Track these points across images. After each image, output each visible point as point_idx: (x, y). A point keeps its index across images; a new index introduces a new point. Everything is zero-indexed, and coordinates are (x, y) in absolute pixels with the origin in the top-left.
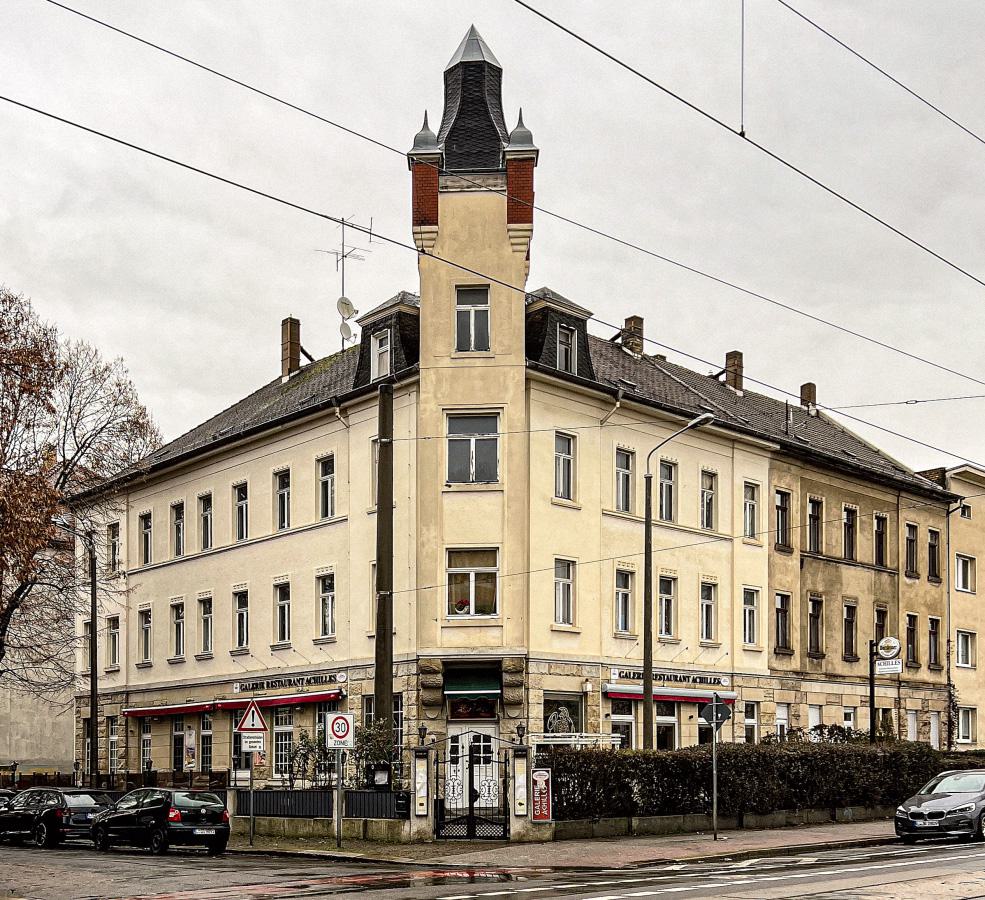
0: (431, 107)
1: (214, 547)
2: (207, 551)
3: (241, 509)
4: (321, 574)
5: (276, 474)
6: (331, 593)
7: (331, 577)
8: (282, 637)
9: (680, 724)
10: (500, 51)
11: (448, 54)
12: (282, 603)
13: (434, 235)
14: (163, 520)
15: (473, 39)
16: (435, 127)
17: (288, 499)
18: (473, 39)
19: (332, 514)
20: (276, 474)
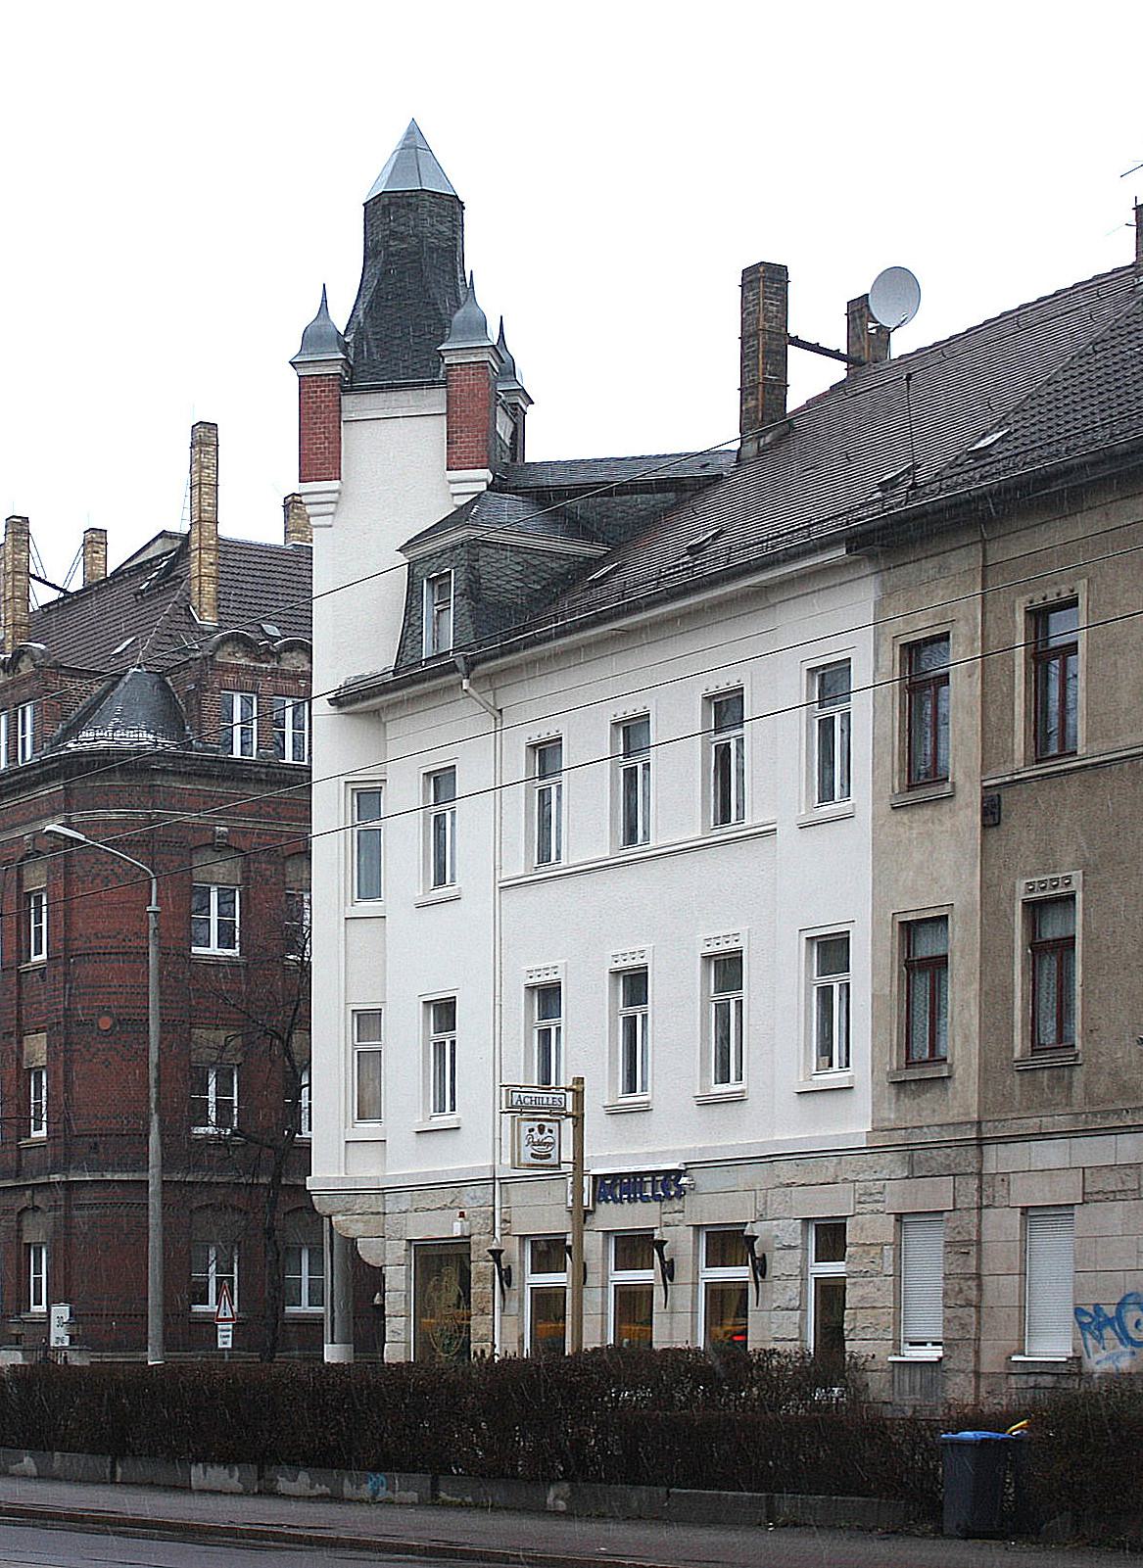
0: (335, 271)
1: (564, 863)
2: (634, 852)
3: (723, 753)
4: (714, 949)
5: (708, 699)
6: (842, 976)
7: (376, 1014)
8: (631, 1088)
9: (696, 1264)
10: (461, 171)
11: (367, 173)
12: (723, 996)
13: (331, 508)
14: (589, 743)
15: (414, 147)
16: (340, 319)
17: (559, 798)
18: (414, 147)
19: (741, 817)
20: (708, 699)
